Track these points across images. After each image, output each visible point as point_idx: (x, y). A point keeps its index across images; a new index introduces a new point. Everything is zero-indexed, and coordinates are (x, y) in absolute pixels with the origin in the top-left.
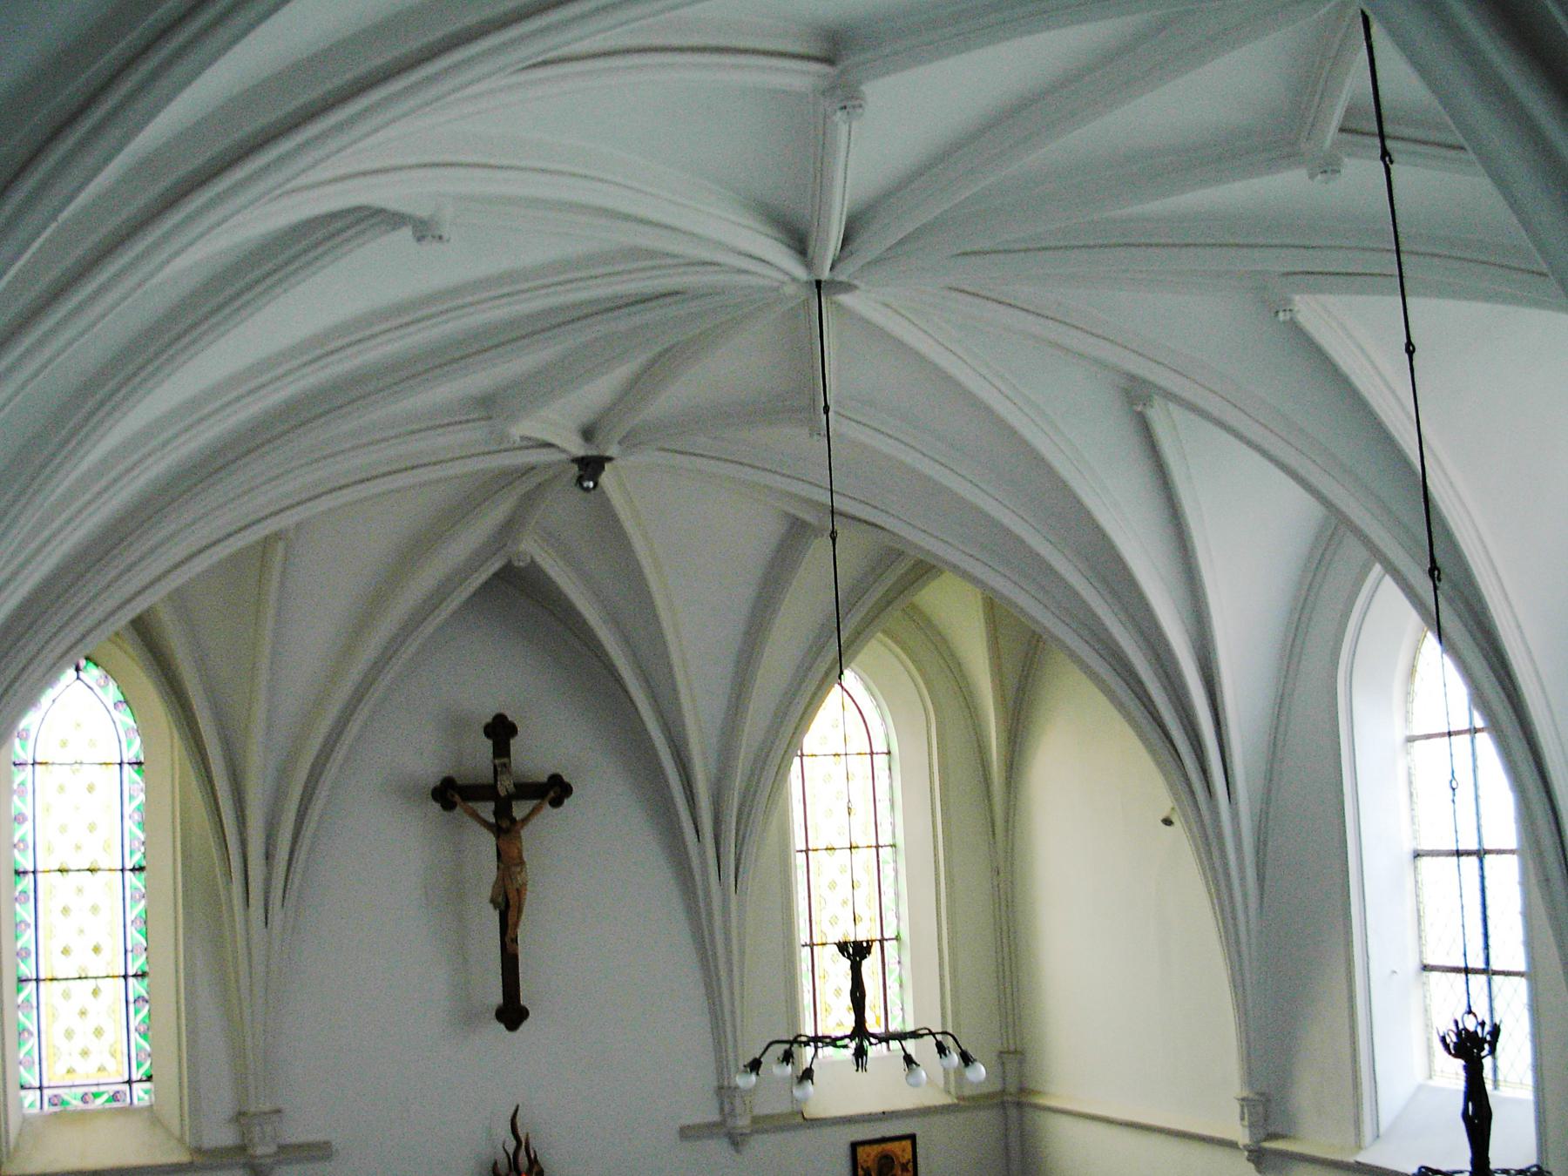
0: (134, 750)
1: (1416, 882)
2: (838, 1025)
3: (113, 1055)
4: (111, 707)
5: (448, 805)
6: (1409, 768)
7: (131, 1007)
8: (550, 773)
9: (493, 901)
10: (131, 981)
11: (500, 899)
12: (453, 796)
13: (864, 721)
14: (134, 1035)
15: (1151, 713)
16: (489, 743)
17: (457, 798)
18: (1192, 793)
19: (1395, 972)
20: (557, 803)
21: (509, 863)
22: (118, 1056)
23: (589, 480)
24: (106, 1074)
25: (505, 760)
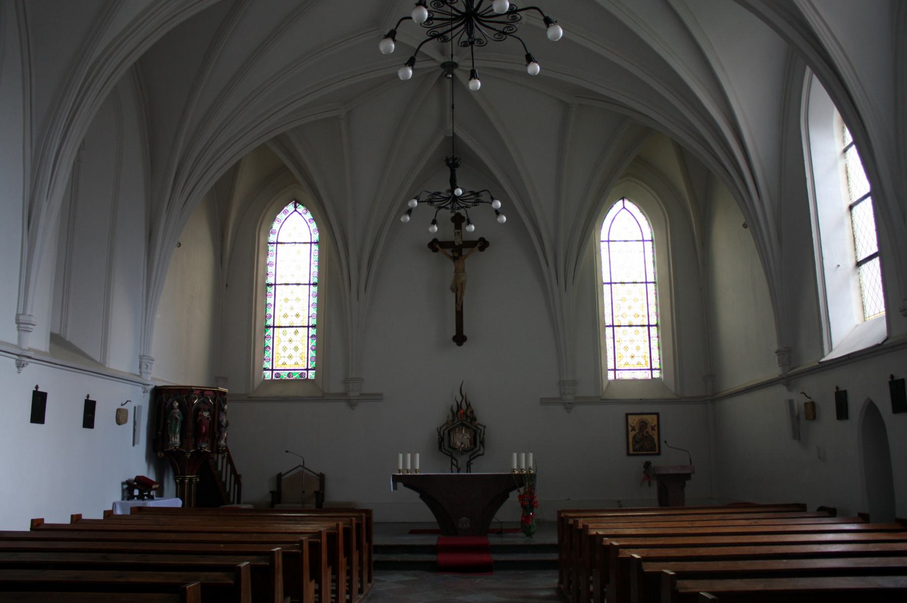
0: (316, 237)
1: (852, 221)
2: (638, 364)
3: (301, 359)
4: (308, 221)
5: (435, 250)
6: (846, 165)
7: (310, 339)
8: (480, 237)
9: (452, 289)
10: (310, 329)
11: (454, 288)
12: (436, 245)
13: (638, 222)
14: (310, 350)
15: (716, 159)
16: (453, 224)
17: (438, 246)
18: (744, 200)
19: (839, 266)
20: (482, 249)
21: (459, 272)
22: (303, 359)
23: (449, 74)
24: (297, 366)
25: (459, 231)
